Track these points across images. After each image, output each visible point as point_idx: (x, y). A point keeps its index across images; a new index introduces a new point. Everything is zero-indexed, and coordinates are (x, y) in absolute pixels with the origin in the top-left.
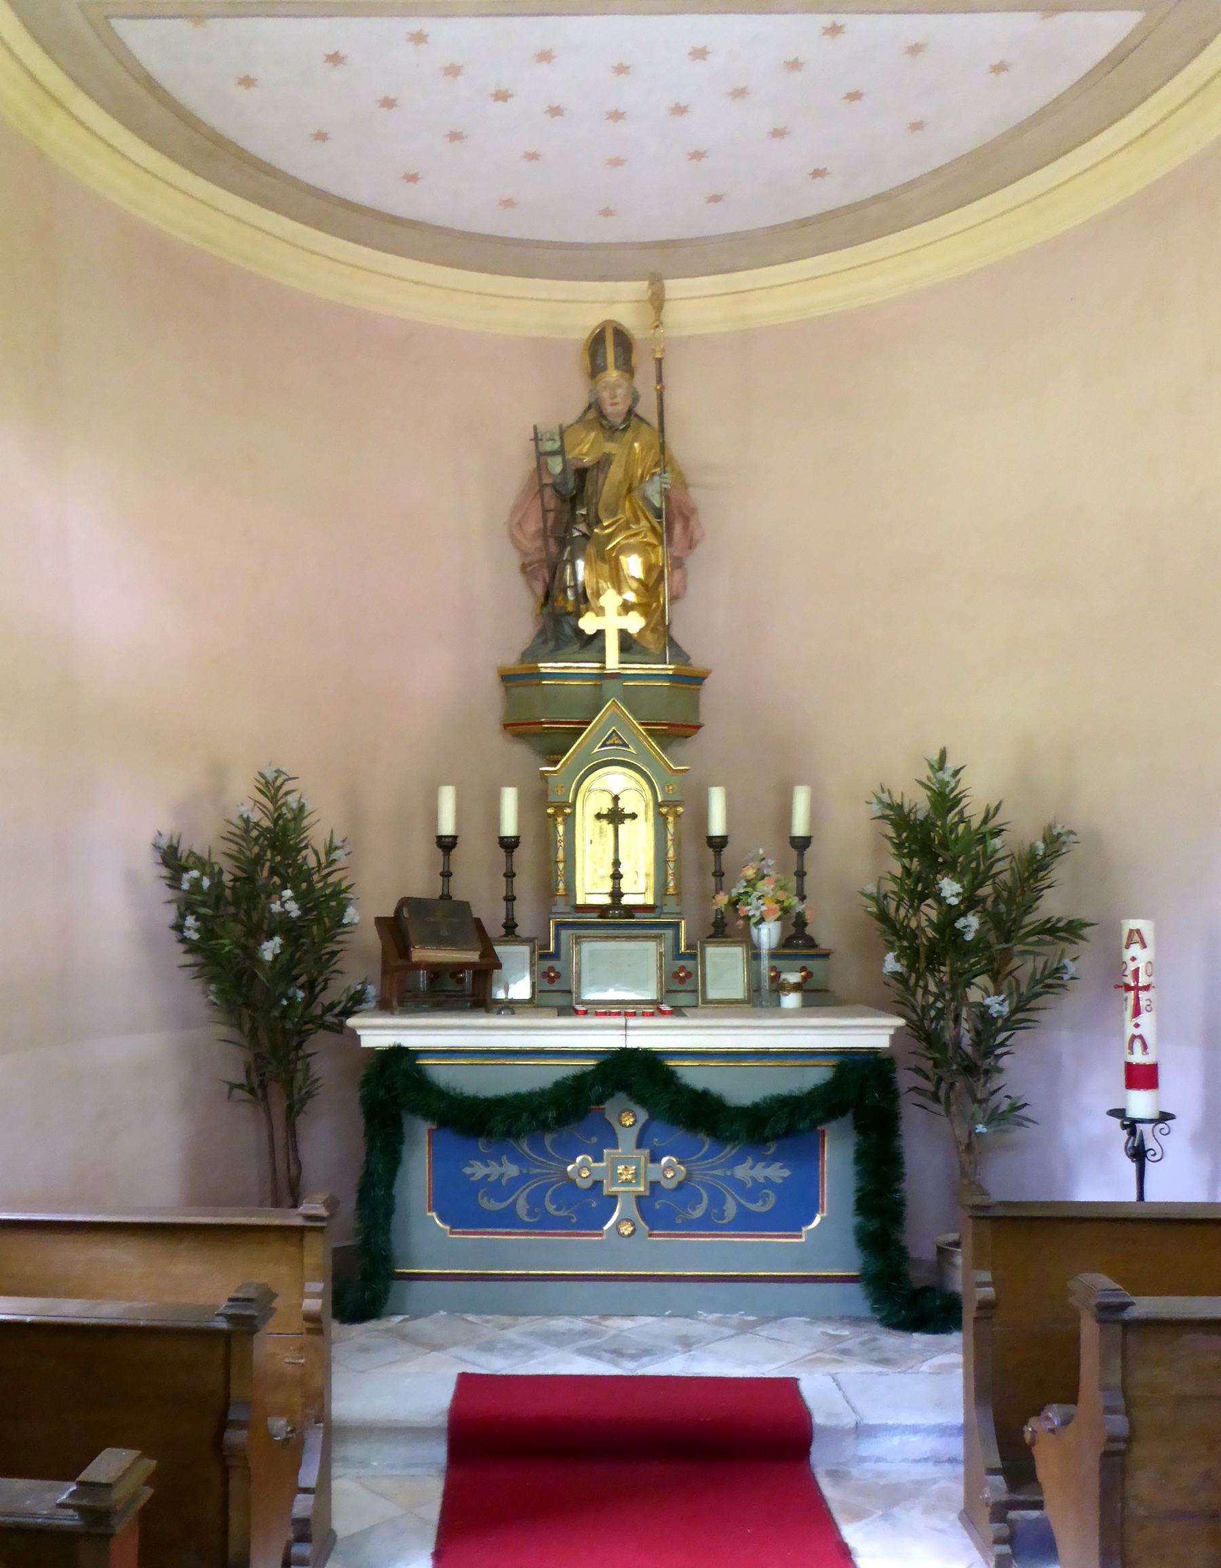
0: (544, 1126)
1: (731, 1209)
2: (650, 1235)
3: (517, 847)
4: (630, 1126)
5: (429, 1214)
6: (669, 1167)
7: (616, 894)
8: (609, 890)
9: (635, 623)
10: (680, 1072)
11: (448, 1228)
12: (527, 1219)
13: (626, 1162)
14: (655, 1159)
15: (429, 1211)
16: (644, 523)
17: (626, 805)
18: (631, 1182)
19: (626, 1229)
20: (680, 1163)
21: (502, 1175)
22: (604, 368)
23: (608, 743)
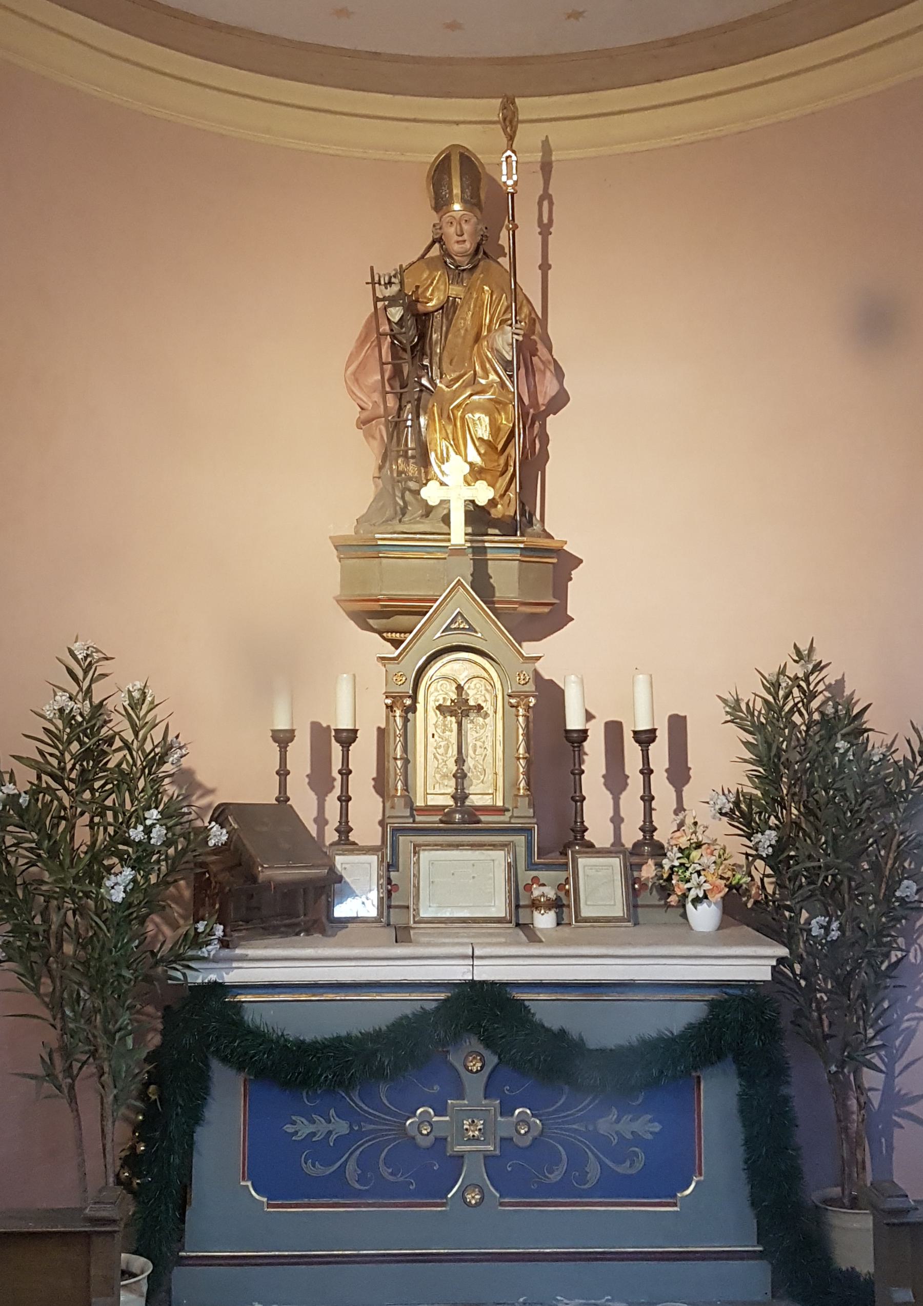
0: (380, 1074)
1: (594, 1172)
2: (501, 1204)
3: (292, 740)
4: (477, 1071)
5: (242, 1183)
6: (522, 1121)
7: (460, 796)
8: (451, 790)
9: (483, 493)
10: (533, 1007)
11: (265, 1200)
12: (357, 1186)
13: (473, 1115)
14: (506, 1111)
15: (244, 1179)
16: (493, 377)
17: (475, 694)
18: (478, 1139)
19: (473, 1197)
20: (534, 1115)
21: (330, 1133)
22: (450, 202)
23: (453, 626)
